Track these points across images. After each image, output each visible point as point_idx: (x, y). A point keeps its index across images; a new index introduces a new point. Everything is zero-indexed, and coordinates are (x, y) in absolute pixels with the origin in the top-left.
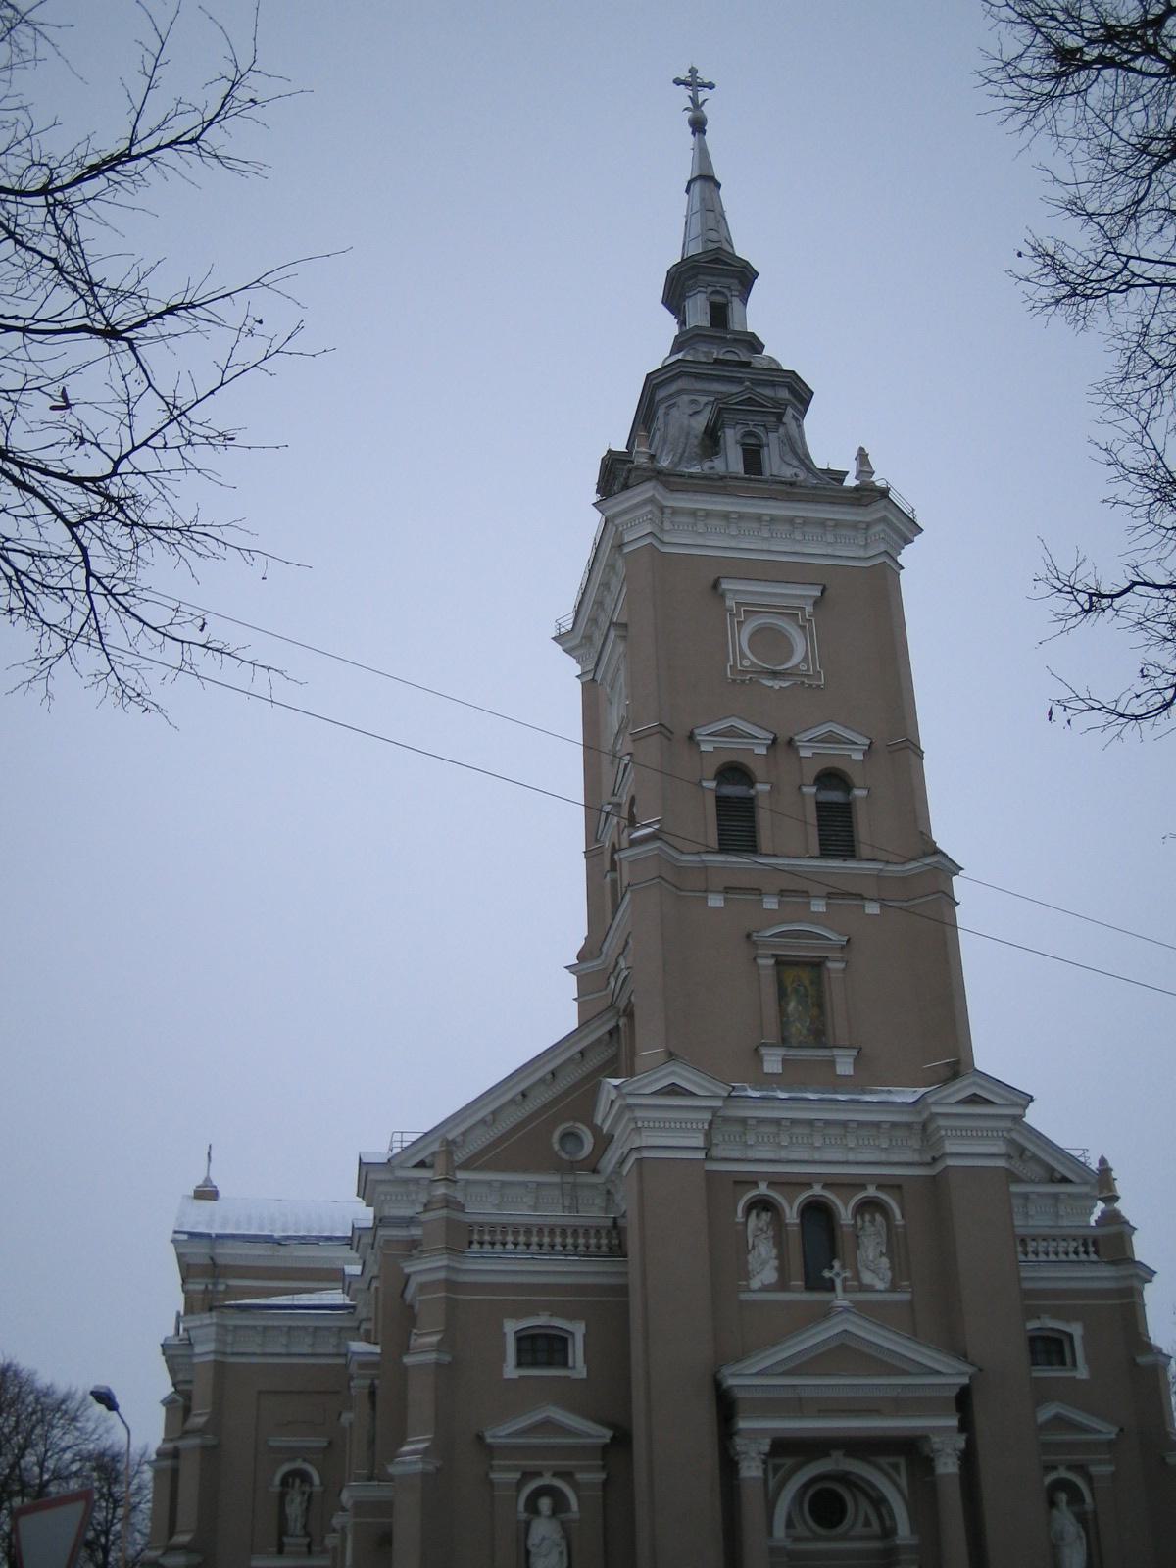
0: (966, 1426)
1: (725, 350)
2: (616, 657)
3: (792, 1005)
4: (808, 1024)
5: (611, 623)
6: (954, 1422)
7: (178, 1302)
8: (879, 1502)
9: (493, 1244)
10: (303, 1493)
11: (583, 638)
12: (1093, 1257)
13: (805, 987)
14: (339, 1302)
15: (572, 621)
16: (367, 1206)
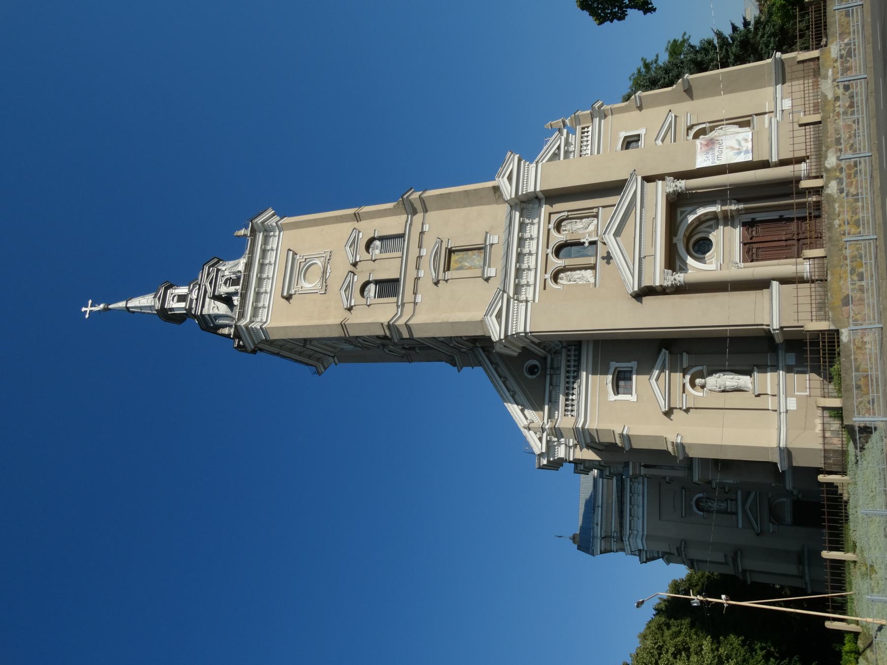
0: (662, 177)
1: (193, 294)
2: (319, 345)
3: (467, 264)
4: (475, 257)
5: (304, 346)
6: (660, 183)
7: (621, 554)
8: (700, 221)
9: (572, 405)
10: (706, 501)
11: (318, 362)
12: (590, 129)
13: (459, 258)
14: (642, 486)
15: (310, 367)
16: (562, 466)
